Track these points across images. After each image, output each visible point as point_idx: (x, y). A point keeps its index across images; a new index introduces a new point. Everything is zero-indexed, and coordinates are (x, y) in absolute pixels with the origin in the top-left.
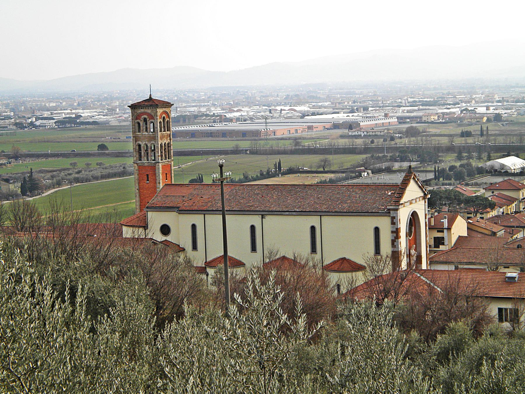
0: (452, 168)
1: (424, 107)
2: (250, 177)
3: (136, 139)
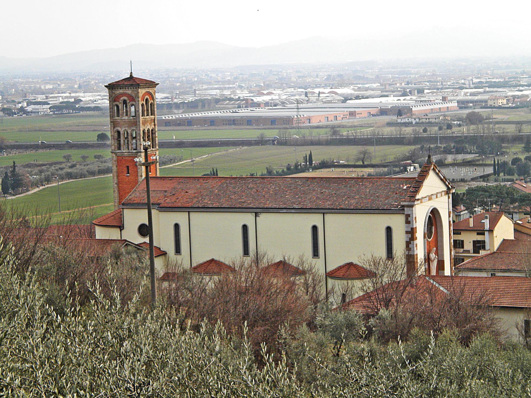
0: (516, 161)
1: (491, 89)
2: (275, 172)
3: (114, 124)
